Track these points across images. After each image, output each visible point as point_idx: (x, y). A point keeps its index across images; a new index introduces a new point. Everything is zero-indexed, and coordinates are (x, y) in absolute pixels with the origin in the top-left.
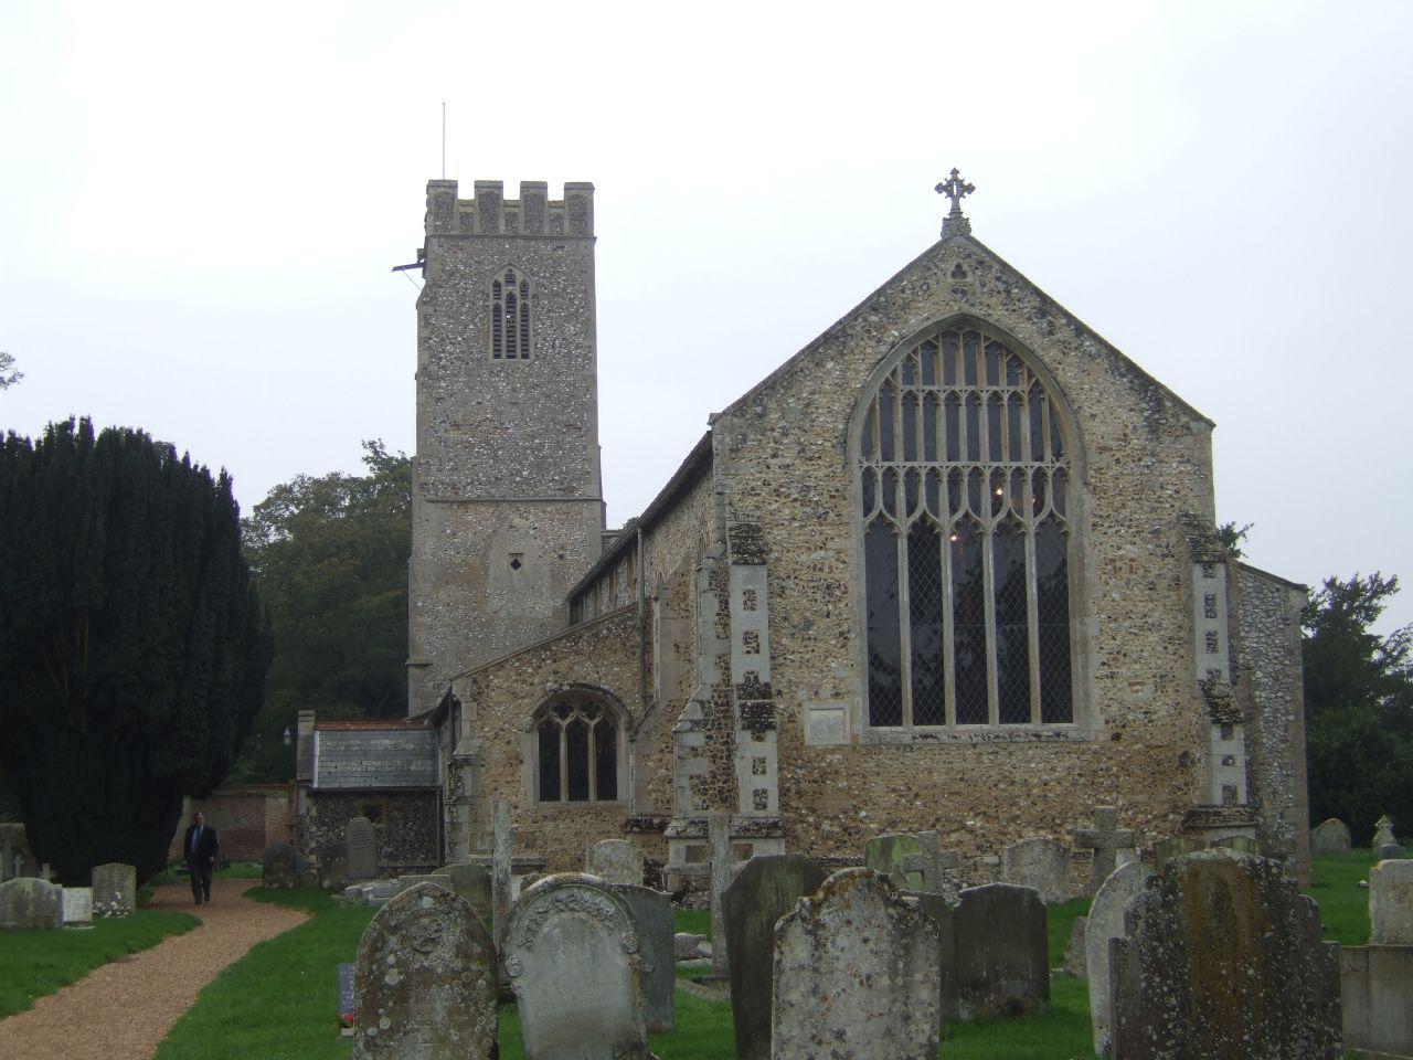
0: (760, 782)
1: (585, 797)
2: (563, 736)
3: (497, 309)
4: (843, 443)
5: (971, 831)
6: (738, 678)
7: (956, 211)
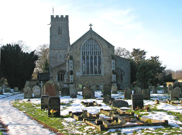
0: (71, 79)
1: (59, 81)
4: (80, 49)
6: (70, 70)
7: (91, 27)
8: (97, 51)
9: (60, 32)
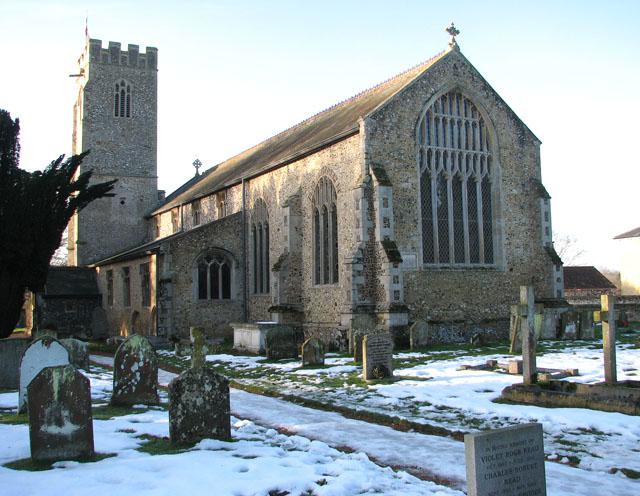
1: (205, 298)
2: (209, 270)
3: (117, 95)
5: (462, 309)
8: (480, 154)
9: (122, 105)
